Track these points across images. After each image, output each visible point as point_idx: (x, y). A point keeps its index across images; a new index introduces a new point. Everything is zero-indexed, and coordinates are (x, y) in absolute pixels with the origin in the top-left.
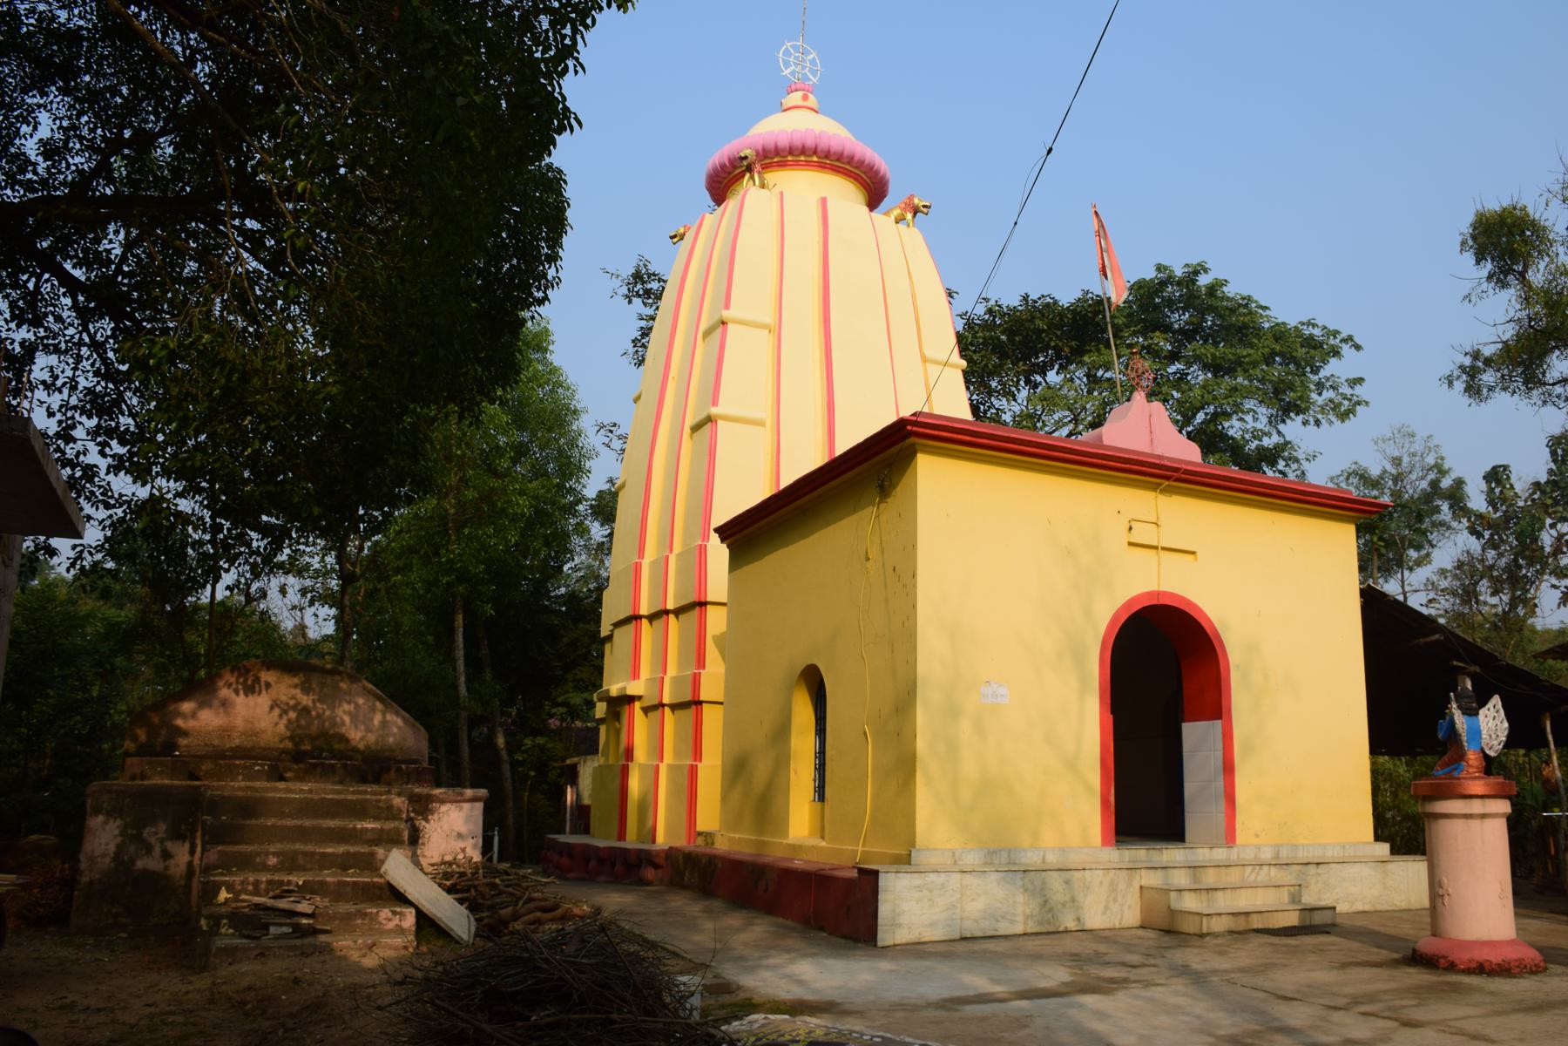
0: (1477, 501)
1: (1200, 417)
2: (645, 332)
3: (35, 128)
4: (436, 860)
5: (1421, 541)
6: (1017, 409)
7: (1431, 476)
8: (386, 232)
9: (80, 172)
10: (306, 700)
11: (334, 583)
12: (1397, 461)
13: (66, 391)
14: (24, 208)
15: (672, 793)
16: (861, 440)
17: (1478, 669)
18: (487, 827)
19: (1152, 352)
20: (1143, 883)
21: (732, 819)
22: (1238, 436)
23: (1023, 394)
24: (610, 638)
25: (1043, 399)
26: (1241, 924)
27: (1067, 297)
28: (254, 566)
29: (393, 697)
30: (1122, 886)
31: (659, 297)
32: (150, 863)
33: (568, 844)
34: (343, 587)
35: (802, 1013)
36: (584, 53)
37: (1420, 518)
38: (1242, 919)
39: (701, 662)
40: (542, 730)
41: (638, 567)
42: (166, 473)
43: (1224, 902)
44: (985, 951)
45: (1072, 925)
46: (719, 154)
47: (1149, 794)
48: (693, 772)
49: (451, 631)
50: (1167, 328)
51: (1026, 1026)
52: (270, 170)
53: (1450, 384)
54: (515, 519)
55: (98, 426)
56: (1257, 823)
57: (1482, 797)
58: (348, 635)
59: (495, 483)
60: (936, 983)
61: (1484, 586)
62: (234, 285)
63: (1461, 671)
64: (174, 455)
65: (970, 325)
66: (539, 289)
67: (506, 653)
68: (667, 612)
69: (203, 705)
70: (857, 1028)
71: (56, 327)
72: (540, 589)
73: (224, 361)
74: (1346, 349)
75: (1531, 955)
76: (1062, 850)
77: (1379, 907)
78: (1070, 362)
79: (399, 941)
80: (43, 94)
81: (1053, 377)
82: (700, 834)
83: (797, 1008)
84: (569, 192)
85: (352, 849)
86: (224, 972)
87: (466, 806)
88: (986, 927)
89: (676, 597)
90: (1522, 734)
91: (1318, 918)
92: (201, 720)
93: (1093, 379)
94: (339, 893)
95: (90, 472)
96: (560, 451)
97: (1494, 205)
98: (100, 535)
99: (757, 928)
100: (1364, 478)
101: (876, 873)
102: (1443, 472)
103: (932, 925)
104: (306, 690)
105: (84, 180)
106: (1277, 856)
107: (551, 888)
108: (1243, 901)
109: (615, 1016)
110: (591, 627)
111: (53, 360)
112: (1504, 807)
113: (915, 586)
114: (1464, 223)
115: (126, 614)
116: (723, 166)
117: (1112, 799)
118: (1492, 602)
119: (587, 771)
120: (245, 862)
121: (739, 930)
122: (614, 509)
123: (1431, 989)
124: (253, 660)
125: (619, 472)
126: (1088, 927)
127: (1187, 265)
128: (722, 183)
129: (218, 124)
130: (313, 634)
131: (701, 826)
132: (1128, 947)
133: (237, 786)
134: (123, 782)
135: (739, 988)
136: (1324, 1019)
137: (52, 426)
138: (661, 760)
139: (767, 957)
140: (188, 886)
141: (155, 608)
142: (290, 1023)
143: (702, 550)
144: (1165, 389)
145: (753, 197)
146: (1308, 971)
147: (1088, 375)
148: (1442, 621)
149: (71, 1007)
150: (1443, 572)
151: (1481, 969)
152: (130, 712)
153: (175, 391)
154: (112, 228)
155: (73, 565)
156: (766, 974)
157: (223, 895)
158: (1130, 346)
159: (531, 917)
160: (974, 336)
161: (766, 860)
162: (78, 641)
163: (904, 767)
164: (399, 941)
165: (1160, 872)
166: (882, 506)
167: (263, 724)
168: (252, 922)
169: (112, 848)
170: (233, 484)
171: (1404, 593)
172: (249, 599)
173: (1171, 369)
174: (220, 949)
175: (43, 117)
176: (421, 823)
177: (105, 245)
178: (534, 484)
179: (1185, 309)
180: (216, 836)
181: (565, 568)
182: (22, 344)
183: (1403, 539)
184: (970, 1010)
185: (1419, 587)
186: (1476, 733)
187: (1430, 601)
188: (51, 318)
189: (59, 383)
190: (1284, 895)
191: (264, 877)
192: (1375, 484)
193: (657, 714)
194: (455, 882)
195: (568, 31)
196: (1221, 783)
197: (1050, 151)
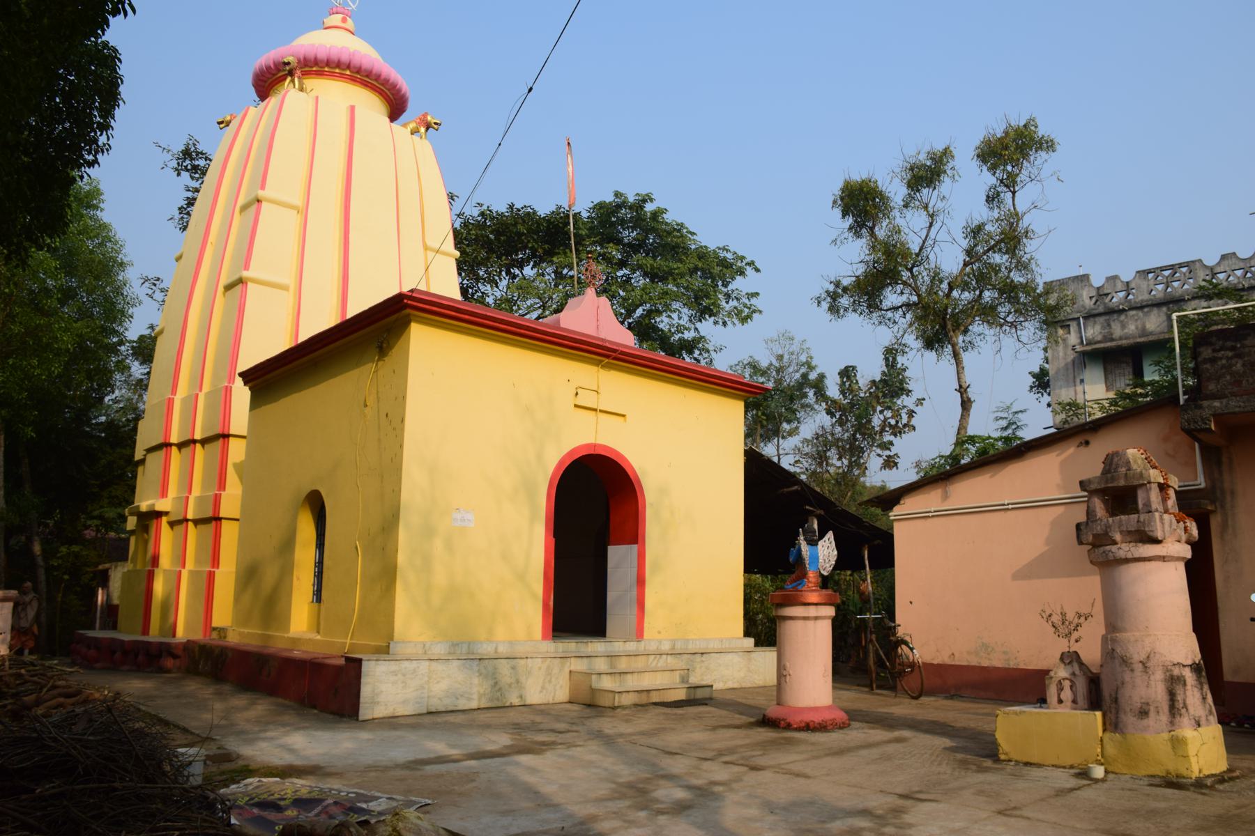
0: (833, 391)
1: (639, 312)
2: (191, 202)
5: (792, 416)
6: (498, 294)
7: (803, 370)
15: (192, 595)
16: (366, 307)
17: (822, 512)
19: (607, 259)
20: (572, 668)
21: (242, 616)
22: (666, 329)
23: (504, 283)
24: (142, 462)
25: (520, 288)
26: (644, 699)
27: (544, 209)
30: (556, 670)
31: (204, 173)
33: (96, 639)
35: (290, 776)
37: (792, 399)
38: (644, 695)
39: (222, 485)
41: (170, 402)
43: (632, 683)
44: (446, 722)
45: (516, 701)
46: (266, 56)
47: (580, 599)
48: (211, 577)
50: (618, 241)
51: (473, 781)
53: (819, 303)
54: (58, 353)
56: (660, 622)
57: (816, 604)
59: (43, 321)
60: (402, 749)
61: (833, 454)
63: (811, 513)
65: (465, 224)
66: (89, 153)
68: (194, 442)
70: (335, 787)
72: (82, 417)
75: (841, 716)
76: (511, 643)
77: (744, 685)
78: (542, 261)
81: (528, 271)
82: (215, 629)
84: (123, 70)
88: (448, 704)
89: (203, 429)
91: (700, 694)
93: (559, 276)
96: (107, 299)
97: (857, 176)
99: (260, 707)
100: (755, 367)
101: (359, 661)
102: (811, 368)
103: (404, 702)
106: (673, 648)
107: (76, 677)
108: (646, 682)
109: (117, 785)
112: (830, 611)
113: (403, 430)
114: (836, 188)
116: (268, 68)
117: (551, 603)
118: (837, 463)
119: (117, 576)
121: (246, 709)
122: (153, 350)
123: (773, 743)
125: (159, 322)
126: (528, 702)
127: (637, 194)
128: (267, 82)
131: (217, 622)
132: (558, 718)
135: (239, 757)
136: (697, 768)
138: (184, 567)
139: (265, 731)
143: (228, 391)
144: (613, 288)
146: (690, 733)
147: (555, 272)
148: (803, 477)
150: (806, 441)
151: (808, 727)
156: (263, 745)
158: (590, 252)
159: (53, 702)
160: (468, 233)
161: (271, 651)
163: (387, 575)
165: (585, 660)
166: (380, 363)
171: (779, 455)
173: (620, 273)
178: (79, 324)
179: (634, 228)
181: (107, 399)
182: (840, 459)
183: (780, 415)
185: (788, 452)
186: (815, 558)
187: (796, 462)
190: (676, 677)
192: (764, 373)
193: (182, 527)
196: (635, 593)
197: (530, 90)
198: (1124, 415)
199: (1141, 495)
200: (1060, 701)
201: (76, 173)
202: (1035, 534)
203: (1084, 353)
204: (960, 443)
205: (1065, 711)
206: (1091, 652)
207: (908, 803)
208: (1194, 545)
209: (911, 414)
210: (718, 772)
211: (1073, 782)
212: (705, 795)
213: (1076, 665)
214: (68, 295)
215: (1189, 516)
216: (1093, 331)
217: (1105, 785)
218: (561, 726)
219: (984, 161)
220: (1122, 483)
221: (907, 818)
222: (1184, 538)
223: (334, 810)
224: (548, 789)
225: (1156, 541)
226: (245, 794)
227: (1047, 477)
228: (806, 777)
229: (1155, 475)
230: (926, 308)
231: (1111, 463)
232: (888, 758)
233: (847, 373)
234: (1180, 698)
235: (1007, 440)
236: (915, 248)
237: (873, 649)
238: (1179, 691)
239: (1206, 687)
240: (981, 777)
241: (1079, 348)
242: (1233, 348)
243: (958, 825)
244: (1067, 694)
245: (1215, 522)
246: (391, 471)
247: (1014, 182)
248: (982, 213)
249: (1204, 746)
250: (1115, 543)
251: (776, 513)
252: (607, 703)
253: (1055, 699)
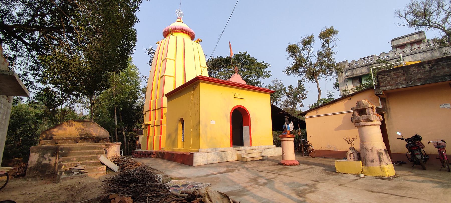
0: (288, 91)
2: (152, 60)
3: (15, 9)
4: (111, 156)
8: (100, 38)
9: (28, 20)
10: (83, 127)
11: (89, 105)
12: (275, 84)
13: (25, 66)
14: (13, 26)
18: (121, 149)
19: (238, 66)
26: (253, 159)
27: (224, 57)
28: (71, 102)
32: (47, 162)
39: (162, 118)
41: (150, 102)
42: (50, 83)
43: (250, 156)
45: (226, 161)
46: (165, 29)
47: (238, 139)
49: (114, 113)
50: (240, 62)
52: (74, 24)
55: (33, 73)
58: (92, 115)
62: (66, 46)
64: (52, 80)
65: (208, 61)
67: (125, 120)
69: (59, 129)
71: (22, 52)
72: (132, 105)
73: (63, 62)
74: (269, 66)
75: (298, 162)
80: (17, 2)
81: (222, 70)
83: (180, 179)
84: (137, 34)
85: (93, 156)
86: (63, 183)
87: (117, 146)
90: (296, 127)
91: (265, 158)
92: (58, 133)
94: (90, 164)
95: (31, 83)
97: (291, 44)
98: (34, 96)
102: (283, 86)
104: (83, 126)
105: (28, 22)
107: (135, 160)
108: (253, 155)
110: (142, 112)
111: (22, 59)
112: (293, 139)
115: (41, 111)
118: (291, 107)
119: (141, 137)
120: (69, 160)
122: (271, 100)
123: (283, 169)
128: (166, 34)
133: (67, 145)
134: (39, 146)
137: (22, 73)
140: (55, 166)
141: (48, 110)
142: (78, 192)
145: (172, 37)
146: (264, 167)
151: (290, 165)
155: (27, 101)
157: (63, 167)
163: (198, 135)
167: (73, 132)
168: (70, 172)
169: (37, 160)
170: (66, 85)
172: (70, 108)
175: (17, 7)
176: (107, 150)
177: (34, 36)
180: (62, 155)
184: (210, 177)
185: (279, 104)
188: (21, 50)
189: (23, 64)
191: (73, 163)
192: (272, 88)
194: (115, 161)
195: (136, 3)
199: (367, 110)
201: (129, 56)
202: (339, 120)
203: (347, 78)
204: (319, 100)
205: (352, 161)
206: (357, 147)
209: (306, 95)
211: (356, 178)
213: (354, 151)
214: (128, 81)
215: (380, 114)
216: (349, 73)
218: (236, 166)
219: (321, 38)
220: (362, 108)
221: (317, 186)
222: (379, 120)
223: (191, 187)
224: (235, 180)
225: (372, 121)
227: (341, 107)
228: (292, 177)
229: (370, 106)
231: (358, 104)
232: (310, 172)
233: (290, 87)
234: (381, 158)
235: (329, 99)
236: (306, 58)
237: (303, 147)
238: (381, 156)
240: (333, 177)
241: (346, 77)
242: (387, 75)
243: (329, 188)
244: (352, 157)
246: (197, 113)
247: (328, 42)
248: (320, 49)
249: (389, 169)
250: (361, 122)
251: (279, 118)
253: (349, 158)
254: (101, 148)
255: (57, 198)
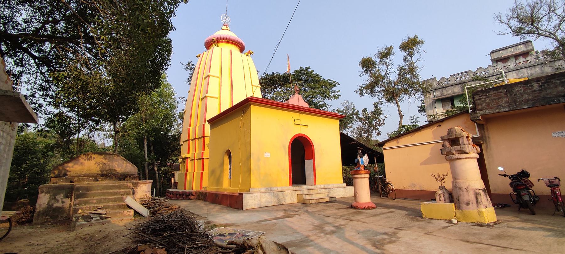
0: (361, 116)
2: (191, 77)
3: (21, 15)
8: (126, 50)
9: (37, 28)
10: (105, 162)
11: (113, 133)
12: (346, 107)
13: (33, 85)
14: (18, 36)
26: (318, 201)
27: (282, 73)
28: (90, 130)
29: (128, 160)
32: (59, 205)
34: (115, 134)
36: (176, 12)
37: (351, 118)
39: (204, 150)
40: (166, 166)
41: (189, 129)
43: (314, 197)
45: (284, 203)
46: (207, 38)
47: (298, 175)
48: (202, 173)
49: (144, 144)
50: (302, 80)
52: (94, 32)
55: (43, 94)
58: (116, 145)
64: (67, 102)
65: (262, 79)
67: (157, 152)
69: (75, 164)
71: (29, 68)
72: (166, 134)
74: (337, 85)
75: (374, 205)
79: (129, 218)
80: (23, 6)
81: (279, 89)
84: (173, 44)
85: (117, 197)
87: (147, 184)
90: (371, 161)
91: (333, 199)
92: (74, 168)
94: (113, 208)
95: (40, 106)
98: (44, 122)
100: (339, 110)
102: (355, 110)
105: (37, 30)
107: (169, 202)
108: (318, 196)
110: (178, 142)
111: (29, 76)
112: (368, 176)
114: (360, 60)
115: (53, 141)
118: (365, 135)
119: (177, 174)
120: (87, 202)
122: (340, 127)
123: (355, 213)
124: (90, 152)
128: (209, 45)
129: (79, 19)
130: (107, 145)
133: (85, 184)
134: (50, 184)
137: (28, 93)
140: (70, 210)
142: (98, 242)
143: (204, 125)
145: (215, 49)
146: (331, 210)
149: (32, 245)
152: (53, 166)
153: (66, 86)
154: (47, 43)
155: (35, 129)
157: (80, 211)
162: (37, 148)
163: (249, 171)
164: (129, 218)
168: (88, 218)
169: (47, 202)
170: (84, 109)
172: (89, 137)
174: (79, 225)
175: (23, 12)
176: (135, 189)
177: (44, 48)
180: (79, 196)
182: (18, 71)
184: (263, 223)
185: (351, 132)
188: (27, 65)
189: (30, 82)
191: (92, 206)
192: (342, 112)
194: (145, 204)
195: (172, 7)
198: (450, 117)
199: (461, 140)
200: (440, 200)
201: (162, 72)
202: (426, 152)
203: (435, 100)
205: (442, 203)
206: (449, 186)
207: (398, 231)
208: (479, 154)
209: (384, 120)
210: (342, 222)
211: (447, 225)
212: (338, 228)
213: (444, 190)
214: (161, 103)
215: (477, 145)
217: (458, 226)
220: (454, 137)
221: (398, 235)
222: (476, 152)
223: (239, 236)
224: (296, 228)
225: (467, 153)
226: (215, 232)
227: (428, 135)
229: (465, 134)
230: (388, 91)
231: (450, 131)
232: (389, 217)
233: (364, 111)
234: (479, 199)
236: (383, 75)
238: (479, 197)
239: (488, 196)
240: (418, 223)
241: (434, 99)
242: (486, 95)
243: (414, 237)
244: (442, 198)
245: (483, 146)
247: (412, 54)
248: (402, 63)
249: (489, 213)
251: (350, 150)
252: (308, 203)
254: (128, 187)
255: (71, 250)
